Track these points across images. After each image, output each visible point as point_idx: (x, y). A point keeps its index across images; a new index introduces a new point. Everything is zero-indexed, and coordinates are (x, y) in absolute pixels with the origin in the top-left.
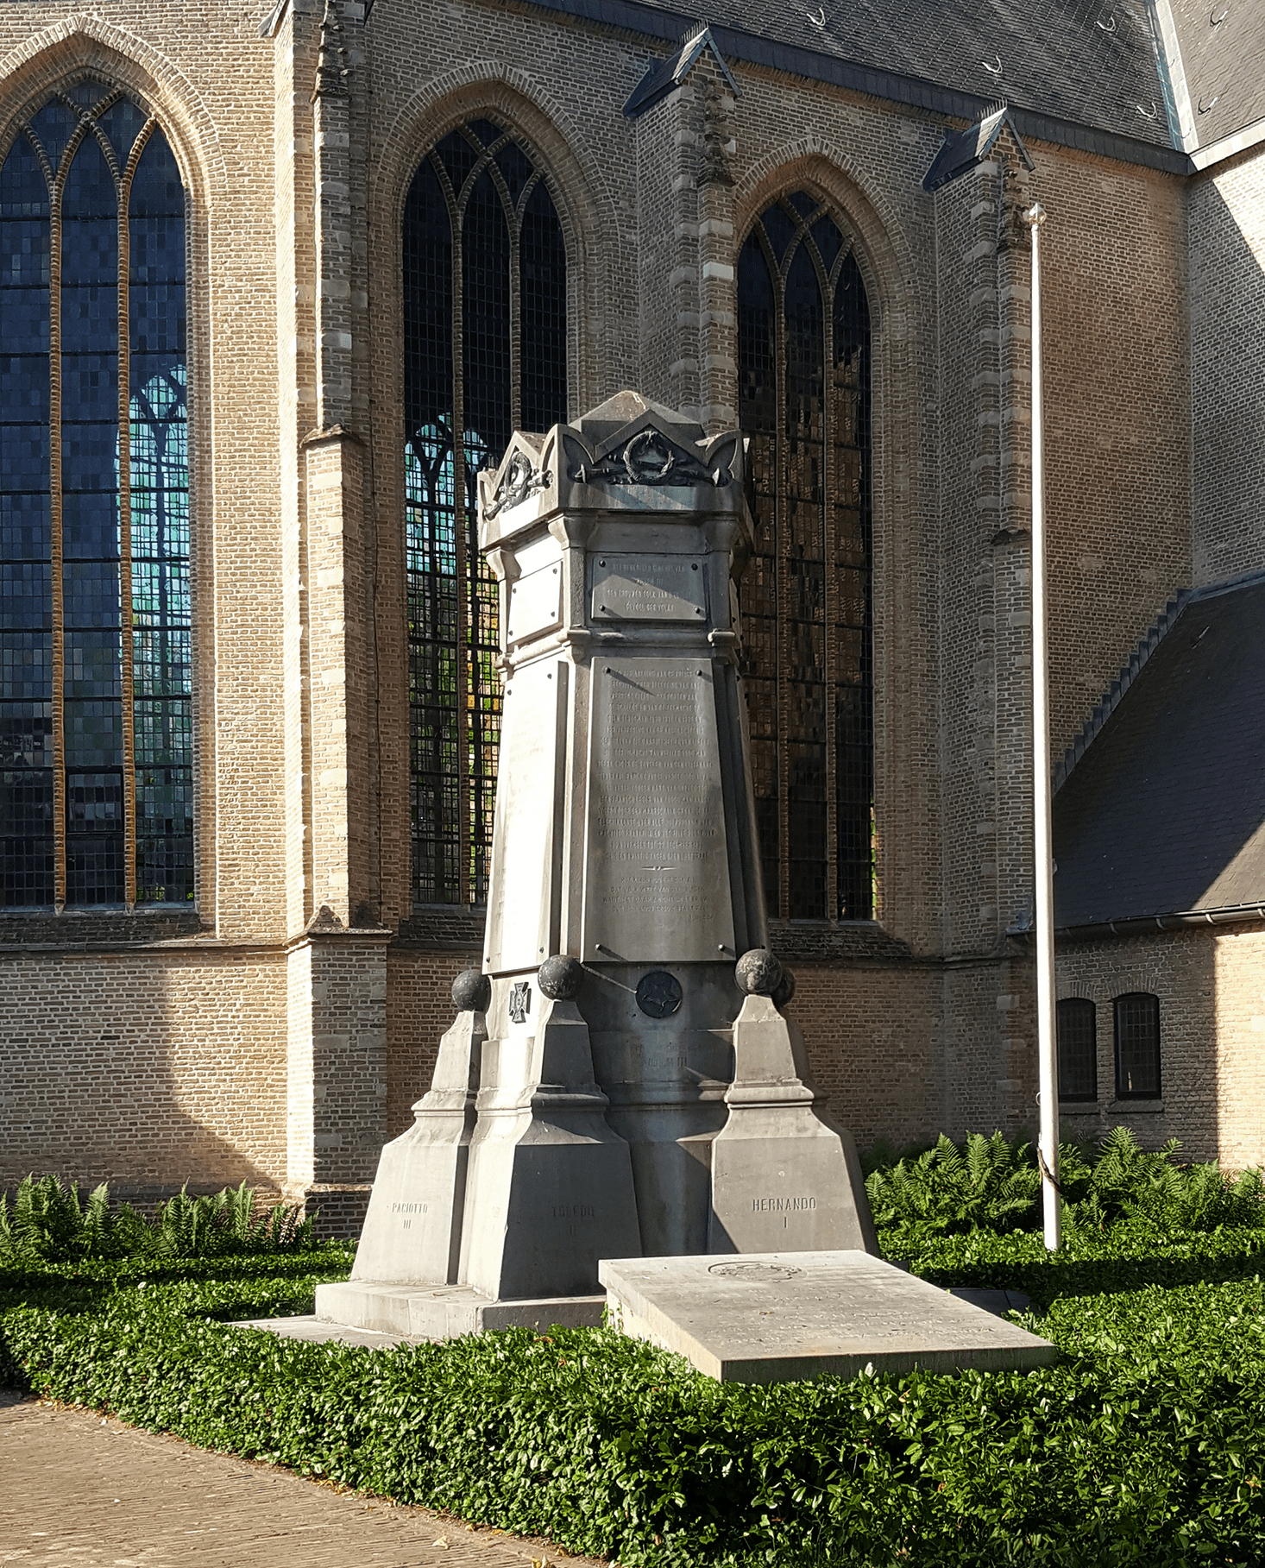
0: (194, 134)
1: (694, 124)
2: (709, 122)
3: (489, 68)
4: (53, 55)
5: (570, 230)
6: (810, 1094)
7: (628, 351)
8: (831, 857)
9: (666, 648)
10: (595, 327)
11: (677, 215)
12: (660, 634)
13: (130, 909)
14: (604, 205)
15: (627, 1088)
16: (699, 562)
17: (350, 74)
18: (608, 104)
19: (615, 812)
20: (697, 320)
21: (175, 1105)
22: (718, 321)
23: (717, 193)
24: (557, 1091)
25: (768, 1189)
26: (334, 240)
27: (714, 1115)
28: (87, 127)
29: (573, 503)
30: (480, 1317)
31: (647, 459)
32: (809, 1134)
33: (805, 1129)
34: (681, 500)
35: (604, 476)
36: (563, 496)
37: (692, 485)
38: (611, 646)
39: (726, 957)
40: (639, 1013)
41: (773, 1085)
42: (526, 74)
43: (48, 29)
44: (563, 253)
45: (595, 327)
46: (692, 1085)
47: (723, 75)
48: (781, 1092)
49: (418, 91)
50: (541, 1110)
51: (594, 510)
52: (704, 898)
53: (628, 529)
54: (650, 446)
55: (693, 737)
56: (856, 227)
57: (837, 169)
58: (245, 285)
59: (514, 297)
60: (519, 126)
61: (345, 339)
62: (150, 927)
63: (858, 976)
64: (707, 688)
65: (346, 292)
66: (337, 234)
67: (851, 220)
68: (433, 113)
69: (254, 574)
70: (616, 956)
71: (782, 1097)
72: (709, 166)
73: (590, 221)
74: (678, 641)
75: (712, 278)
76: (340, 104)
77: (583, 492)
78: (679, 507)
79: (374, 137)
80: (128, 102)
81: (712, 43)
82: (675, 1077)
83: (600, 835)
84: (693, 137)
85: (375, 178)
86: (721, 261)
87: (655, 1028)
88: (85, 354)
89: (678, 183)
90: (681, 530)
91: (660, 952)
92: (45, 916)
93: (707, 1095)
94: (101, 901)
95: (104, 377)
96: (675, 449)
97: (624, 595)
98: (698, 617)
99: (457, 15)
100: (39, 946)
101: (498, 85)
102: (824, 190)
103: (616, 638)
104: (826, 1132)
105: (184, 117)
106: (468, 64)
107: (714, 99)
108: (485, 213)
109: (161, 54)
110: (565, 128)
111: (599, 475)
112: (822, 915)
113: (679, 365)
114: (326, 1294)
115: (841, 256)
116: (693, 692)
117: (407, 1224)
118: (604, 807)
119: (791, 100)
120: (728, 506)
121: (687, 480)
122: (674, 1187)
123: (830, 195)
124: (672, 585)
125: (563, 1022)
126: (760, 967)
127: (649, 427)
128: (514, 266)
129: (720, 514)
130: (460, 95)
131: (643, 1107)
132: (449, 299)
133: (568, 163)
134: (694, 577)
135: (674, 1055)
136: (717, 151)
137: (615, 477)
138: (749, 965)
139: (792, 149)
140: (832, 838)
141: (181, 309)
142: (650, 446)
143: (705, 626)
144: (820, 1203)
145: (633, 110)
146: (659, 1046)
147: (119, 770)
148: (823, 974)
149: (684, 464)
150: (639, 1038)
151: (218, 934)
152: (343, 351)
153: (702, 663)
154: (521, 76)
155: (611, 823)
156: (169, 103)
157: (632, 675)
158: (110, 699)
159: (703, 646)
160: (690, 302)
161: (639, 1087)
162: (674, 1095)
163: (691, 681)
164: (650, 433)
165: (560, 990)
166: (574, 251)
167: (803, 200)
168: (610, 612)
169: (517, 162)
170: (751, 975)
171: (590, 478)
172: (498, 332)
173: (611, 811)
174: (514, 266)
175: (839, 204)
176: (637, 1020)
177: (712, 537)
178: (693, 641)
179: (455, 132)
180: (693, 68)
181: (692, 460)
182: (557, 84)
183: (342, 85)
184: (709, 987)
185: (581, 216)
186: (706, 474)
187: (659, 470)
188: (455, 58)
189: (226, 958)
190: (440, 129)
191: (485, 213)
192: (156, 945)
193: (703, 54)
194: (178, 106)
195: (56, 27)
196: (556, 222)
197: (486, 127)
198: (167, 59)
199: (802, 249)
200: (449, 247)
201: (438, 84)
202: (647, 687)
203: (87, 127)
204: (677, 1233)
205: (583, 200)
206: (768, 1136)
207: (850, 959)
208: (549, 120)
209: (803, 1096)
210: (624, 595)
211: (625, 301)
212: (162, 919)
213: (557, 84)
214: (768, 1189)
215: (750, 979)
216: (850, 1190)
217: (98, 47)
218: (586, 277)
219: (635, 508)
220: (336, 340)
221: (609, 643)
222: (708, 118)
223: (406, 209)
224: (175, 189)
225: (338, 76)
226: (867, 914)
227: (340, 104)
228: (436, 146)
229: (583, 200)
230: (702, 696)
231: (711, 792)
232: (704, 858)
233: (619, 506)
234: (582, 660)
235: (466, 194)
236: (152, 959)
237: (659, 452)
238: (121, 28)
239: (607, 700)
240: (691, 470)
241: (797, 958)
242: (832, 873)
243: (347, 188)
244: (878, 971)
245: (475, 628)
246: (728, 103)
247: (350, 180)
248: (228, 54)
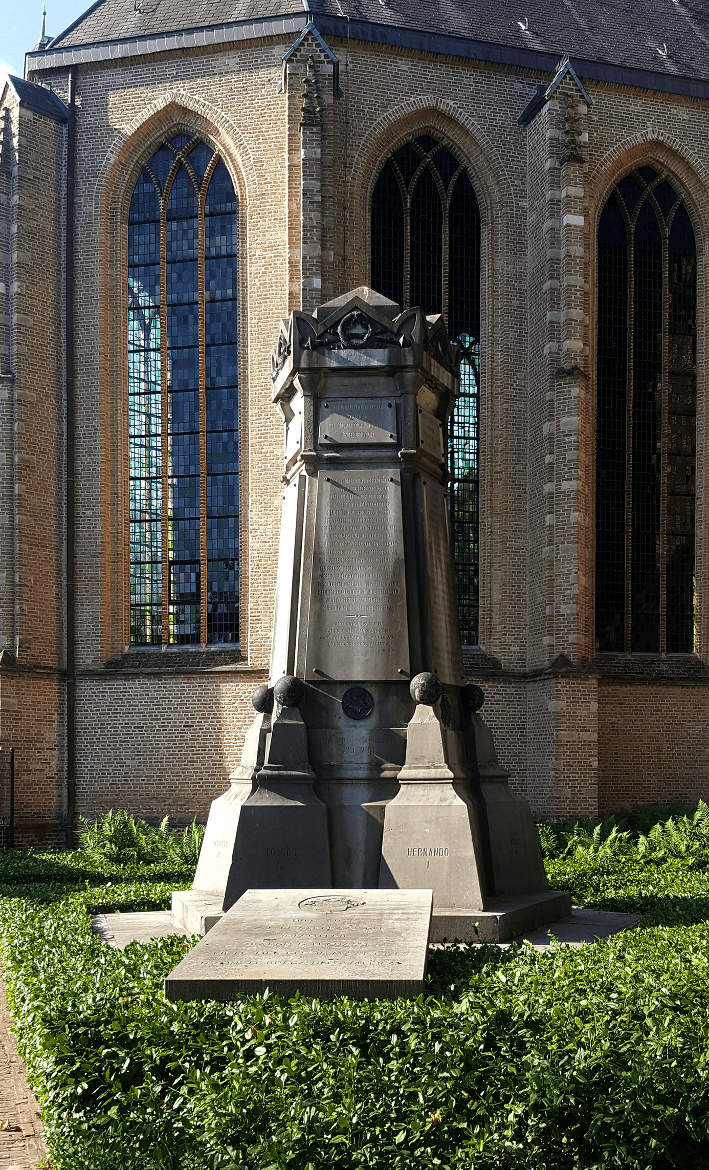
0: (239, 159)
1: (558, 125)
2: (569, 123)
3: (426, 100)
4: (160, 117)
5: (483, 202)
6: (451, 775)
7: (520, 278)
8: (662, 610)
9: (370, 463)
10: (499, 264)
11: (547, 186)
12: (366, 454)
13: (203, 648)
14: (503, 184)
15: (331, 768)
16: (393, 402)
17: (321, 110)
18: (507, 118)
19: (330, 578)
20: (560, 255)
21: (224, 768)
22: (572, 254)
23: (572, 170)
24: (278, 769)
25: (418, 841)
26: (311, 219)
27: (391, 788)
28: (180, 162)
29: (303, 365)
30: (203, 923)
31: (355, 331)
32: (447, 803)
33: (446, 799)
34: (376, 358)
35: (323, 345)
36: (296, 361)
37: (385, 347)
38: (333, 463)
39: (404, 678)
40: (343, 716)
41: (429, 768)
42: (451, 103)
43: (155, 102)
44: (479, 219)
45: (499, 264)
46: (376, 767)
47: (579, 91)
48: (433, 773)
49: (378, 120)
50: (259, 783)
51: (319, 369)
52: (389, 637)
53: (345, 381)
54: (356, 321)
55: (385, 524)
56: (685, 187)
57: (670, 149)
58: (268, 254)
59: (445, 249)
60: (449, 138)
61: (317, 282)
62: (213, 658)
63: (678, 690)
64: (396, 490)
65: (318, 251)
66: (312, 215)
67: (682, 183)
68: (391, 131)
69: (272, 437)
70: (327, 677)
71: (433, 776)
72: (568, 152)
73: (496, 196)
74: (378, 458)
75: (568, 225)
76: (315, 130)
77: (310, 357)
78: (376, 363)
79: (349, 151)
80: (204, 143)
81: (571, 70)
82: (365, 760)
83: (319, 592)
84: (558, 133)
85: (349, 178)
86: (575, 213)
87: (354, 726)
88: (180, 305)
89: (548, 165)
90: (382, 380)
91: (358, 673)
92: (156, 652)
93: (387, 774)
94: (188, 643)
95: (191, 317)
96: (373, 323)
97: (340, 427)
98: (391, 441)
99: (405, 68)
100: (149, 670)
101: (433, 111)
102: (662, 164)
103: (335, 457)
104: (459, 802)
105: (235, 151)
106: (412, 99)
107: (572, 107)
108: (426, 196)
109: (219, 111)
110: (478, 136)
111: (321, 344)
112: (657, 651)
113: (548, 284)
114: (178, 897)
115: (676, 207)
116: (386, 493)
117: (218, 854)
118: (322, 575)
119: (637, 106)
120: (410, 361)
121: (382, 344)
122: (359, 836)
123: (666, 167)
124: (375, 419)
125: (287, 722)
126: (423, 685)
127: (356, 308)
128: (445, 230)
129: (406, 367)
130: (408, 120)
131: (341, 781)
132: (402, 253)
133: (481, 158)
134: (390, 413)
135: (365, 745)
136: (573, 141)
137: (332, 344)
138: (417, 682)
139: (638, 137)
140: (663, 597)
141: (235, 272)
142: (356, 321)
143: (397, 446)
144: (452, 852)
145: (525, 120)
146: (355, 739)
147: (198, 562)
148: (652, 689)
149: (381, 333)
150: (341, 733)
151: (249, 663)
152: (315, 290)
153: (393, 472)
154: (448, 104)
155: (327, 587)
156: (226, 142)
157: (345, 482)
158: (193, 519)
159: (395, 461)
160: (555, 241)
161: (339, 767)
162: (363, 773)
163: (385, 486)
164: (355, 313)
165: (285, 700)
166: (486, 216)
167: (648, 172)
168: (331, 439)
169: (448, 160)
170: (417, 690)
171: (315, 347)
172: (655, 299)
173: (327, 579)
174: (445, 230)
175: (673, 173)
176: (342, 721)
177: (402, 383)
178: (389, 458)
179: (407, 144)
180: (558, 87)
181: (386, 330)
182: (470, 107)
183: (321, 118)
184: (393, 699)
185: (491, 191)
186: (395, 340)
187: (362, 338)
188: (396, 95)
189: (254, 677)
190: (395, 143)
191: (426, 196)
192: (213, 670)
193: (565, 78)
194: (230, 143)
195: (160, 100)
196: (474, 198)
197: (427, 140)
198: (223, 114)
199: (647, 205)
200: (402, 219)
201: (393, 113)
202: (355, 491)
203: (180, 162)
204: (358, 868)
205: (491, 182)
206: (421, 804)
207: (670, 679)
208: (467, 131)
209: (447, 776)
210: (340, 427)
211: (518, 246)
212: (219, 653)
213: (470, 107)
214: (418, 841)
215: (417, 693)
216: (471, 843)
217: (185, 111)
218: (493, 232)
219: (346, 365)
220: (311, 283)
221: (331, 460)
222: (567, 120)
223: (373, 197)
224: (231, 196)
225: (314, 112)
226: (689, 647)
227: (315, 130)
228: (393, 155)
229: (491, 182)
230: (392, 495)
231: (397, 561)
232: (390, 609)
233: (334, 364)
234: (312, 474)
235: (413, 184)
236: (212, 678)
237: (363, 325)
238: (196, 97)
239: (326, 500)
240: (384, 337)
241: (633, 678)
242: (663, 621)
243: (319, 184)
244: (693, 687)
245: (453, 468)
246: (583, 109)
247: (322, 180)
248: (259, 107)
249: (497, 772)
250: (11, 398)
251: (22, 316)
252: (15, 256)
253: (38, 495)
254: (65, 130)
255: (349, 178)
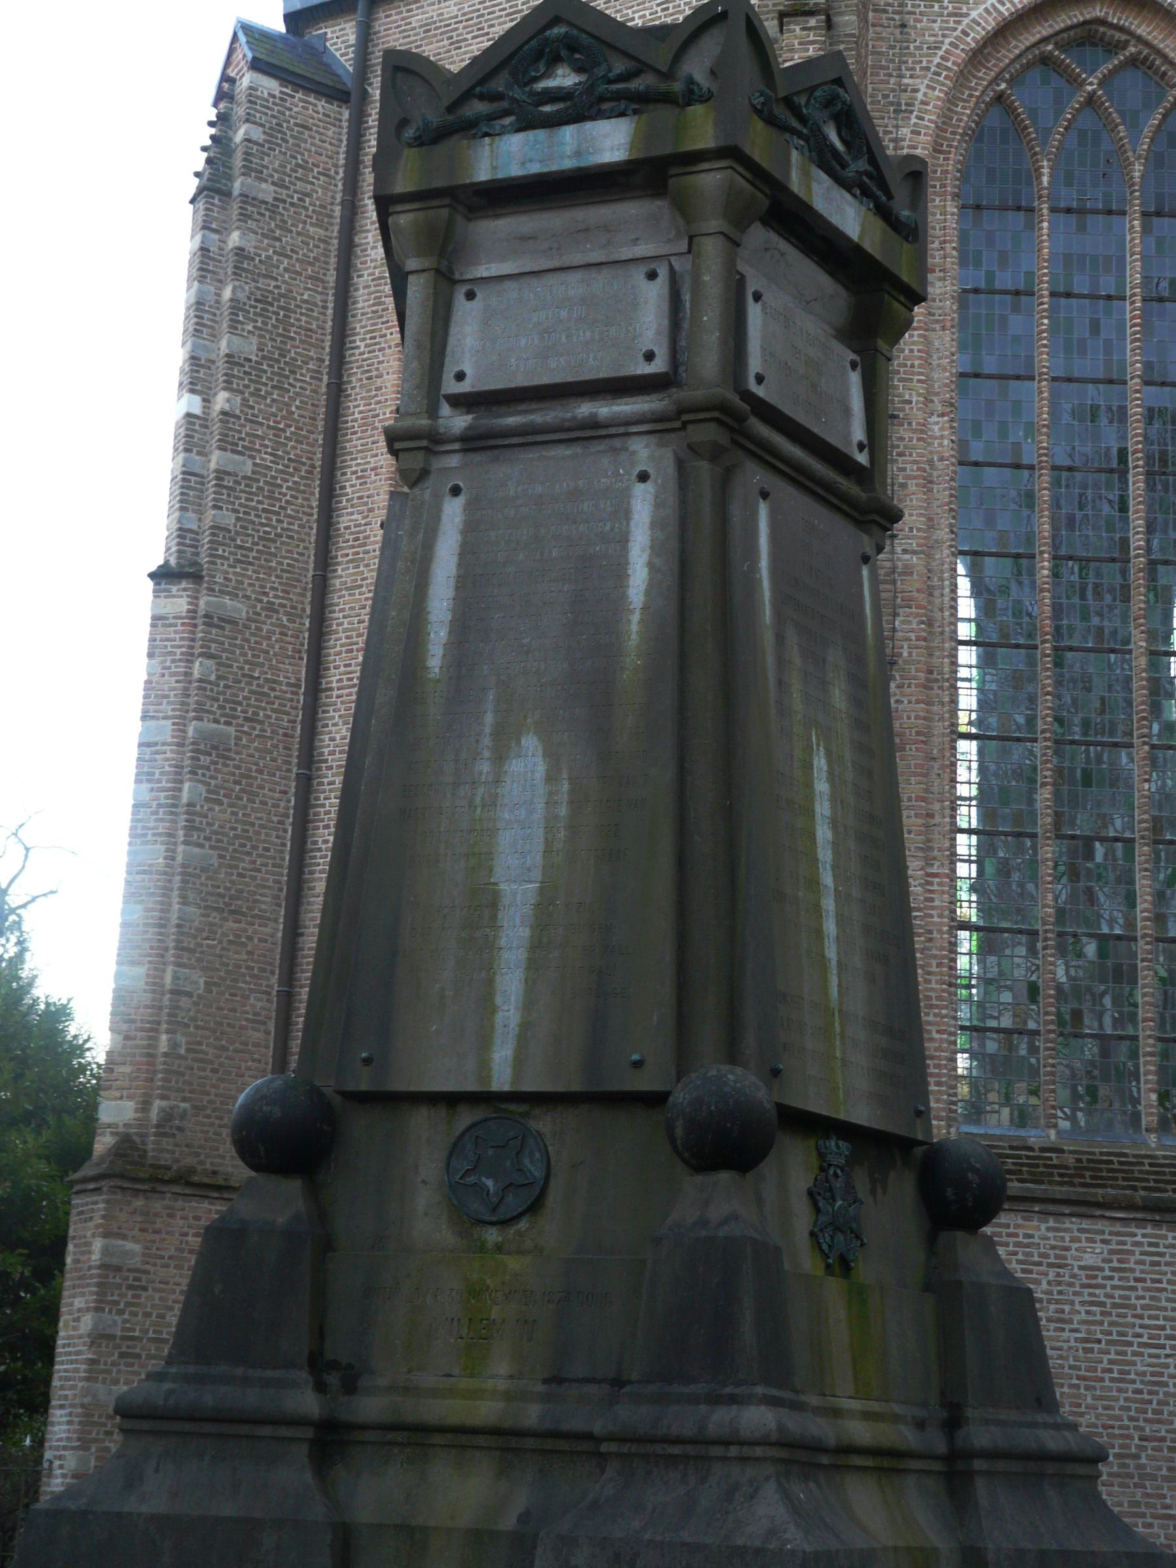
34: (610, 141)
55: (618, 602)
79: (906, 81)
85: (905, 131)
90: (630, 210)
178: (641, 420)
227: (812, 22)
240: (637, 84)
249: (1053, 1441)
250: (193, 612)
251: (229, 454)
252: (224, 343)
253: (231, 805)
254: (346, 114)
255: (905, 131)
